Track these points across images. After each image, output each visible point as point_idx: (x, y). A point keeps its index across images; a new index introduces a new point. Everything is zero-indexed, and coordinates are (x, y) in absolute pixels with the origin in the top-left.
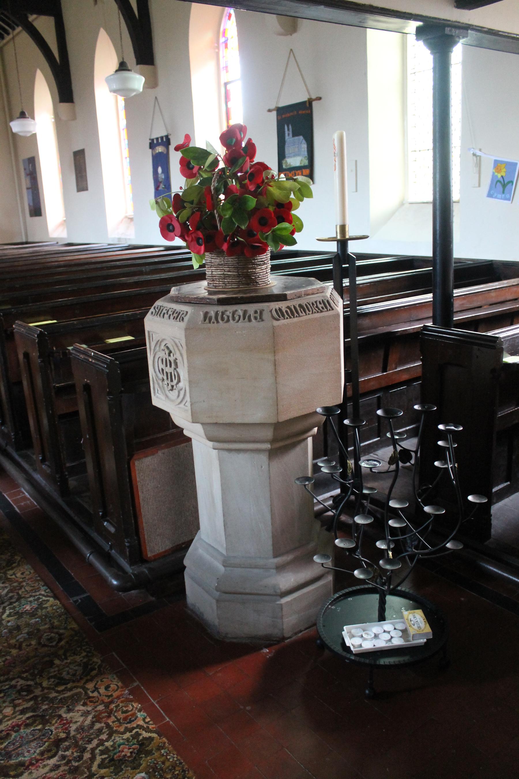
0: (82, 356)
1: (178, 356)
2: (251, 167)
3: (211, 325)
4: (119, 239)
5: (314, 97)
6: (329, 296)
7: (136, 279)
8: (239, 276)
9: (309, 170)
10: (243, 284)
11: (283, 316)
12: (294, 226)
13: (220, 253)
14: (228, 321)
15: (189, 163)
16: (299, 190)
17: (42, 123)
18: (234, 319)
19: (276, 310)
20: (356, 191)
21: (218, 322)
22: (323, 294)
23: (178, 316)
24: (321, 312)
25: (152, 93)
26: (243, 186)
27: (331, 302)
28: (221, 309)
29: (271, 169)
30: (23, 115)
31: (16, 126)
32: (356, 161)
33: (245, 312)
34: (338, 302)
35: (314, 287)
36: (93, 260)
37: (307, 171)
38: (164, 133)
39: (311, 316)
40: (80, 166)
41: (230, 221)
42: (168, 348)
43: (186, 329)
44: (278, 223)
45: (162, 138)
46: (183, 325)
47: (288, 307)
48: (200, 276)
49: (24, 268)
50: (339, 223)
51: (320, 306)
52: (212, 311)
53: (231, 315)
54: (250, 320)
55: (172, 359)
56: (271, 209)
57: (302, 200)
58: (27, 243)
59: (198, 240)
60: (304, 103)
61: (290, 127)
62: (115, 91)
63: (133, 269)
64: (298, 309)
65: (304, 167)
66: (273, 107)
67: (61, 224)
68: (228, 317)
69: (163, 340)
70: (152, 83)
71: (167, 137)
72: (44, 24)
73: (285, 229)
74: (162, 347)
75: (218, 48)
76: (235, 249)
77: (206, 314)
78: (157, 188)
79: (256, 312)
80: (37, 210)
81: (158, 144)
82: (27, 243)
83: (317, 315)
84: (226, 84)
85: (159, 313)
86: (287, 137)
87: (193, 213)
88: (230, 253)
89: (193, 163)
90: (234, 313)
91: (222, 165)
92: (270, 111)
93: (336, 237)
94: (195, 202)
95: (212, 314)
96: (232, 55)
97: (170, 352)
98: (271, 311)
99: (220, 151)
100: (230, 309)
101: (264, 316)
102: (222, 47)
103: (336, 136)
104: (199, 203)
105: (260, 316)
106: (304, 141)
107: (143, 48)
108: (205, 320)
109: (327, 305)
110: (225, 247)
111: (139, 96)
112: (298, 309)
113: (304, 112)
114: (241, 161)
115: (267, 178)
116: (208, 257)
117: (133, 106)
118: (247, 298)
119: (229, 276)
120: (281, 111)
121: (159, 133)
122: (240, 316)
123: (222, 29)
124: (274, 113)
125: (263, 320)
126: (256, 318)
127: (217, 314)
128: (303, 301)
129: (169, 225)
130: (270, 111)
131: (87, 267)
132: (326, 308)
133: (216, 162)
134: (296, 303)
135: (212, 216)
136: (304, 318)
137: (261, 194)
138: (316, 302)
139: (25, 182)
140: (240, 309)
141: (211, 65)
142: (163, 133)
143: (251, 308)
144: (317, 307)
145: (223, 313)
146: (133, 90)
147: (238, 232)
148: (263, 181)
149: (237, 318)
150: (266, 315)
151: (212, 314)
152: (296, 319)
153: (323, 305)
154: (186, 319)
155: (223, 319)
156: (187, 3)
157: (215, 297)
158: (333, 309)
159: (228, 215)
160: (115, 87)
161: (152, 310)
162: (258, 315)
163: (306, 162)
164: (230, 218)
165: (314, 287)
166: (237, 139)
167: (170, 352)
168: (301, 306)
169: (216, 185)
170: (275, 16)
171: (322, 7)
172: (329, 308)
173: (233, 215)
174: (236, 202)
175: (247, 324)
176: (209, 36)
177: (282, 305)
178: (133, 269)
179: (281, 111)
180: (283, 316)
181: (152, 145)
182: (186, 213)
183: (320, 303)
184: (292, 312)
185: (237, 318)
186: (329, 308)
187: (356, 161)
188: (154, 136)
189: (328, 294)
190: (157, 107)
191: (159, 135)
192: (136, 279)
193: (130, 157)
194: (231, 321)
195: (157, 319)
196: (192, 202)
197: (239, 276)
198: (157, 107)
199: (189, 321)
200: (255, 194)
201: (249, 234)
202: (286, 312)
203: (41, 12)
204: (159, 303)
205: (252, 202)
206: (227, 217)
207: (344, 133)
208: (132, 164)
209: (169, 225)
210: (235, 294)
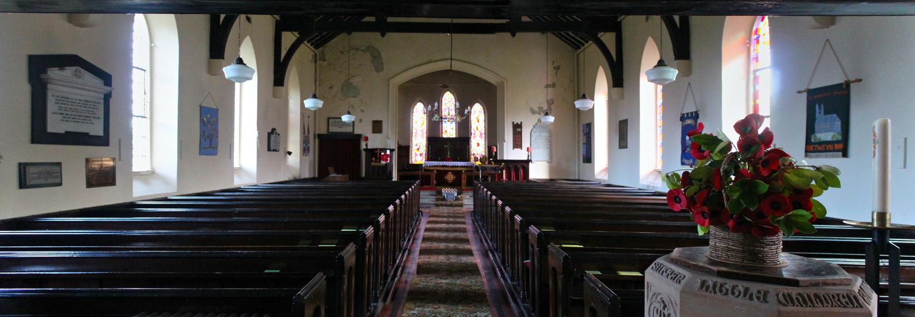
0: (592, 285)
1: (672, 311)
2: (766, 154)
3: (708, 293)
4: (648, 186)
5: (851, 79)
6: (857, 291)
7: (654, 222)
8: (744, 252)
9: (842, 147)
10: (748, 260)
11: (793, 302)
12: (812, 213)
13: (725, 228)
14: (726, 294)
15: (700, 147)
16: (823, 179)
17: (599, 103)
18: (733, 293)
19: (784, 295)
20: (905, 167)
21: (715, 292)
22: (849, 288)
23: (676, 278)
24: (845, 307)
25: (686, 80)
26: (755, 169)
27: (860, 299)
28: (720, 281)
29: (788, 156)
30: (584, 97)
31: (578, 104)
32: (906, 139)
33: (747, 290)
34: (870, 298)
35: (837, 277)
36: (623, 201)
37: (841, 146)
38: (694, 110)
39: (830, 309)
40: (623, 132)
41: (738, 201)
42: (663, 302)
43: (682, 292)
44: (795, 208)
45: (692, 113)
46: (679, 287)
47: (799, 294)
48: (704, 241)
49: (571, 200)
50: (877, 208)
51: (843, 301)
52: (711, 280)
53: (730, 289)
54: (751, 298)
55: (666, 312)
56: (787, 194)
57: (826, 189)
58: (578, 180)
59: (703, 213)
60: (841, 85)
61: (822, 106)
62: (652, 81)
63: (654, 213)
64: (813, 298)
65: (837, 142)
66: (804, 88)
67: (605, 170)
68: (727, 290)
69: (659, 294)
70: (686, 73)
71: (696, 113)
72: (608, 39)
73: (802, 216)
74: (659, 299)
75: (750, 43)
76: (740, 226)
77: (703, 283)
78: (683, 151)
79: (759, 292)
80: (588, 158)
81: (688, 118)
82: (578, 180)
83: (837, 309)
84: (755, 71)
85: (659, 269)
86: (817, 115)
87: (701, 189)
88: (735, 229)
89: (703, 148)
90: (734, 288)
91: (734, 150)
92: (799, 92)
93: (872, 223)
94: (704, 179)
95: (710, 283)
96: (764, 49)
97: (665, 306)
98: (777, 295)
99: (734, 138)
100: (729, 283)
101: (769, 298)
102: (753, 42)
103: (877, 124)
104: (708, 181)
105: (764, 297)
106: (838, 119)
107: (681, 48)
108: (702, 287)
109: (853, 301)
110: (730, 223)
111: (673, 84)
112: (813, 298)
113: (840, 93)
114: (754, 148)
115: (784, 165)
116: (712, 229)
117: (669, 91)
118: (750, 276)
119: (733, 250)
120: (811, 93)
121: (690, 109)
122: (740, 292)
123: (754, 29)
124: (805, 94)
125: (766, 302)
126: (758, 298)
127: (715, 285)
128: (821, 291)
129: (676, 197)
130: (799, 92)
131: (616, 206)
132: (852, 303)
133: (729, 145)
134: (811, 291)
135: (720, 193)
136: (820, 309)
137: (776, 179)
138: (838, 295)
139: (582, 139)
140: (741, 285)
141: (741, 60)
142: (692, 109)
143: (754, 287)
144: (839, 300)
145: (722, 285)
146: (667, 80)
147: (746, 211)
148: (779, 167)
149: (737, 293)
150: (771, 298)
151: (710, 283)
152: (808, 309)
153: (847, 300)
154: (683, 282)
155: (721, 291)
156: (720, 17)
157: (715, 268)
158: (861, 307)
159: (735, 196)
160: (652, 78)
161: (653, 265)
162: (761, 296)
163: (840, 138)
164: (738, 199)
165: (837, 277)
166: (752, 128)
167: (665, 306)
168: (816, 295)
169: (726, 167)
170: (811, 18)
171: (865, 3)
172: (856, 304)
173: (741, 197)
174: (746, 184)
175: (748, 302)
176: (741, 35)
177: (793, 291)
178: (654, 213)
179: (811, 93)
180: (793, 302)
181: (683, 118)
182: (693, 189)
183: (844, 297)
184: (804, 301)
185: (737, 293)
186: (856, 304)
187: (906, 139)
188: (685, 112)
189: (856, 289)
190: (689, 91)
191: (689, 111)
192: (654, 222)
193: (663, 126)
194: (730, 295)
195: (657, 274)
196: (700, 180)
197: (744, 252)
198: (689, 91)
199: (686, 284)
200: (767, 180)
201: (759, 215)
202: (797, 299)
203: (606, 30)
204: (660, 260)
205: (764, 187)
206: (735, 198)
207: (889, 121)
208: (664, 132)
209: (676, 197)
210: (738, 269)
